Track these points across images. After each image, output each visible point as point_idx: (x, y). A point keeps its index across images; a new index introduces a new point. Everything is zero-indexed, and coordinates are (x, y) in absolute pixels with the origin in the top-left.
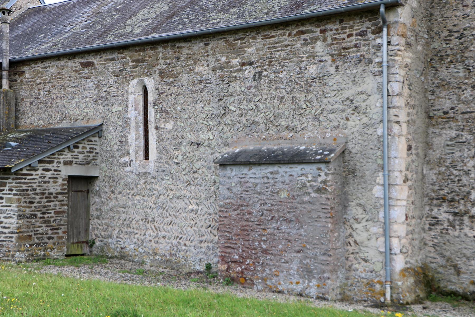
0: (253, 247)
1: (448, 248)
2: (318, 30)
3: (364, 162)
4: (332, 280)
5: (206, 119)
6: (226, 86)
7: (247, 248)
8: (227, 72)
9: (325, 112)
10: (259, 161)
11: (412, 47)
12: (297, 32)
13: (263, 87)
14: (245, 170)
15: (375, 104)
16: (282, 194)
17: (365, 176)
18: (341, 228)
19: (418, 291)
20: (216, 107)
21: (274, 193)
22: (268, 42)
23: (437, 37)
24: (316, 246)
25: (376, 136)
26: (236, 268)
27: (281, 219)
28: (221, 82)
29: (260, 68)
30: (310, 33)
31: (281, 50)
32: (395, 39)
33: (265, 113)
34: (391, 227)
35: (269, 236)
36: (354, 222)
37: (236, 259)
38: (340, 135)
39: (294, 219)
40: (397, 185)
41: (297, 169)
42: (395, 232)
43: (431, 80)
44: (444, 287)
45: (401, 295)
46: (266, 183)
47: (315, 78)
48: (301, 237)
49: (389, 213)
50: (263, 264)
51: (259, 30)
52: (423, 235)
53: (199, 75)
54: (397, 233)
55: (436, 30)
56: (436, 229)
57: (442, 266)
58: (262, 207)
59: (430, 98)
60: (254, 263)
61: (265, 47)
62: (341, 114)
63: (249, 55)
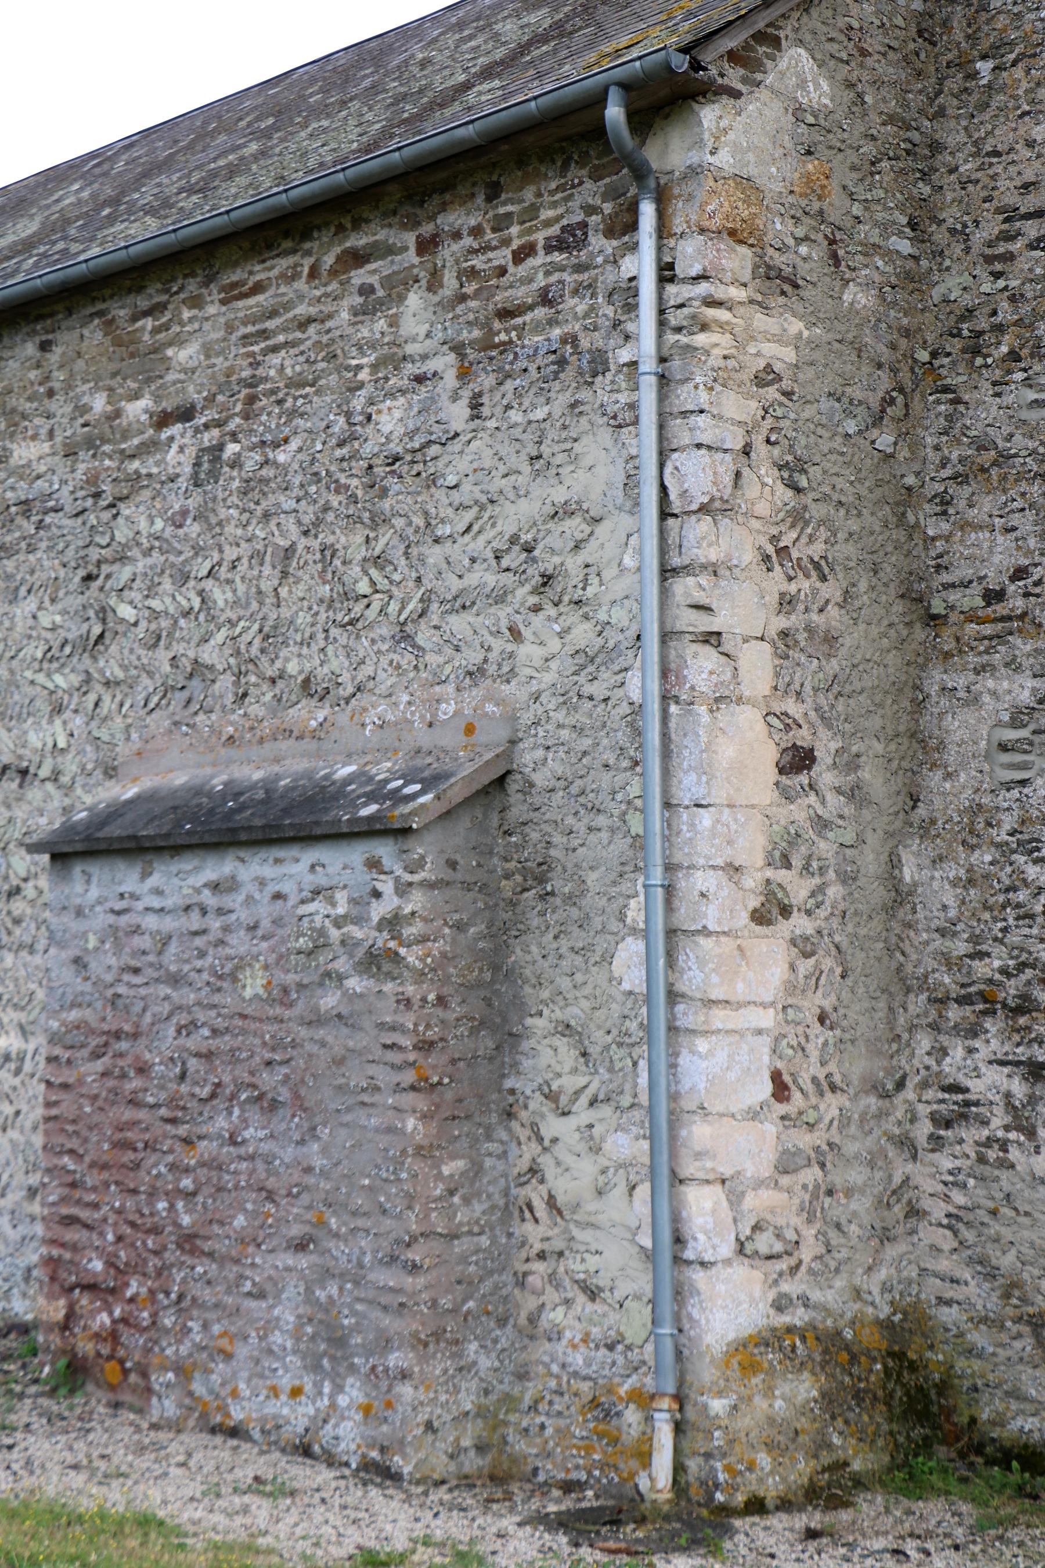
0: (149, 1222)
1: (1007, 1233)
2: (410, 238)
3: (581, 827)
4: (425, 1383)
5: (45, 665)
6: (106, 516)
7: (133, 1225)
8: (111, 458)
9: (435, 606)
10: (168, 835)
11: (808, 293)
12: (338, 259)
13: (223, 513)
14: (128, 877)
15: (622, 554)
16: (249, 981)
17: (583, 893)
18: (489, 1138)
19: (836, 1440)
20: (76, 612)
21: (220, 977)
22: (241, 314)
23: (958, 249)
24: (360, 1222)
25: (625, 709)
26: (94, 1313)
27: (243, 1097)
28: (90, 502)
29: (216, 432)
30: (382, 257)
31: (286, 344)
32: (690, 250)
33: (232, 624)
34: (684, 1133)
35: (202, 1173)
36: (547, 1107)
37: (95, 1274)
38: (490, 708)
39: (284, 1094)
40: (705, 932)
41: (294, 869)
42: (698, 1155)
43: (937, 448)
44: (993, 1423)
45: (719, 1465)
46: (196, 933)
47: (397, 459)
48: (311, 1180)
49: (673, 1066)
50: (181, 1297)
51: (211, 266)
52: (901, 1169)
53: (22, 478)
54: (709, 1164)
55: (951, 215)
56: (961, 1142)
57: (984, 1320)
58: (181, 1041)
59: (931, 532)
60: (152, 1292)
61: (233, 338)
62: (493, 610)
63: (182, 376)
